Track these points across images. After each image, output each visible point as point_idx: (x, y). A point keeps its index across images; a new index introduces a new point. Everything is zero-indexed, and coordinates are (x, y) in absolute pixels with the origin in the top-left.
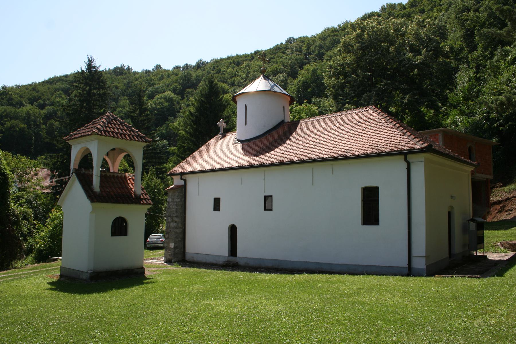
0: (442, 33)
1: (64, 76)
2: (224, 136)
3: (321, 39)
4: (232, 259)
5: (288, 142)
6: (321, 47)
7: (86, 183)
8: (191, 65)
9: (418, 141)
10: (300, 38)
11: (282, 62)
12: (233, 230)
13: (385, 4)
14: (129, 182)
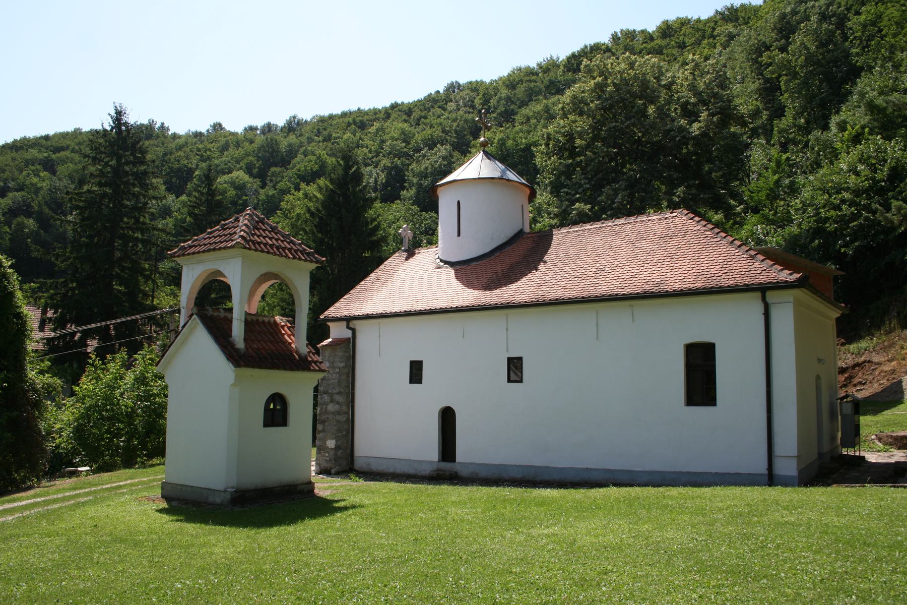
0: (723, 83)
1: (41, 137)
2: (410, 254)
3: (507, 86)
4: (446, 466)
5: (542, 266)
6: (508, 99)
7: (219, 331)
9: (782, 270)
10: (471, 83)
11: (441, 124)
12: (447, 417)
13: (618, 31)
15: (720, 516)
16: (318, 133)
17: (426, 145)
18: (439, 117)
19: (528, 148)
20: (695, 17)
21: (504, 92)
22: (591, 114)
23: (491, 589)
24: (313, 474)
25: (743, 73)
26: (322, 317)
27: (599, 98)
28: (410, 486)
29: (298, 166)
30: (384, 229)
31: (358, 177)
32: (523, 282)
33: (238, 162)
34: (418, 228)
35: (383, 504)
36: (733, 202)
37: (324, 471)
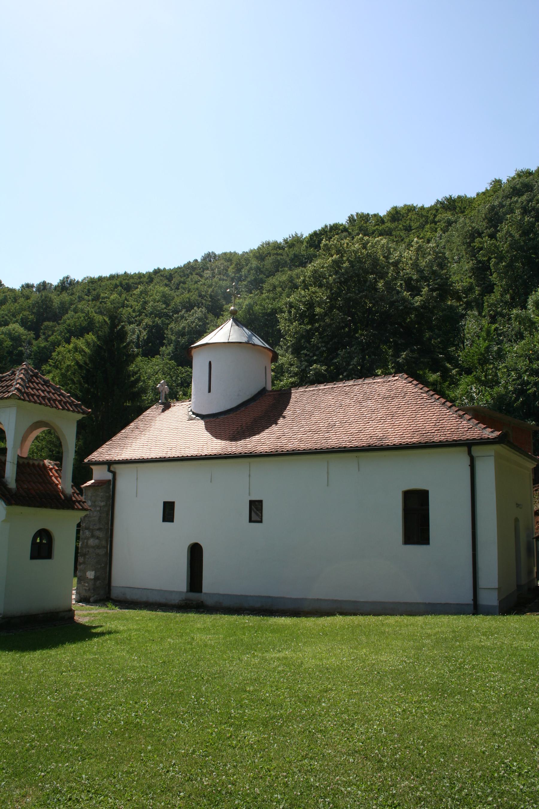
0: (441, 262)
2: (167, 407)
3: (257, 258)
4: (194, 596)
5: (281, 421)
6: (258, 270)
8: (51, 284)
9: (485, 428)
10: (225, 254)
11: (197, 289)
12: (195, 552)
14: (51, 474)
15: (427, 641)
16: (89, 293)
17: (184, 307)
18: (196, 282)
19: (274, 312)
20: (420, 205)
21: (254, 263)
22: (329, 287)
23: (227, 705)
24: (74, 602)
25: (459, 254)
26: (86, 461)
27: (336, 273)
28: (160, 613)
29: (68, 321)
30: (144, 381)
31: (122, 335)
32: (265, 434)
33: (14, 316)
34: (175, 381)
35: (136, 630)
36: (449, 365)
37: (83, 600)
